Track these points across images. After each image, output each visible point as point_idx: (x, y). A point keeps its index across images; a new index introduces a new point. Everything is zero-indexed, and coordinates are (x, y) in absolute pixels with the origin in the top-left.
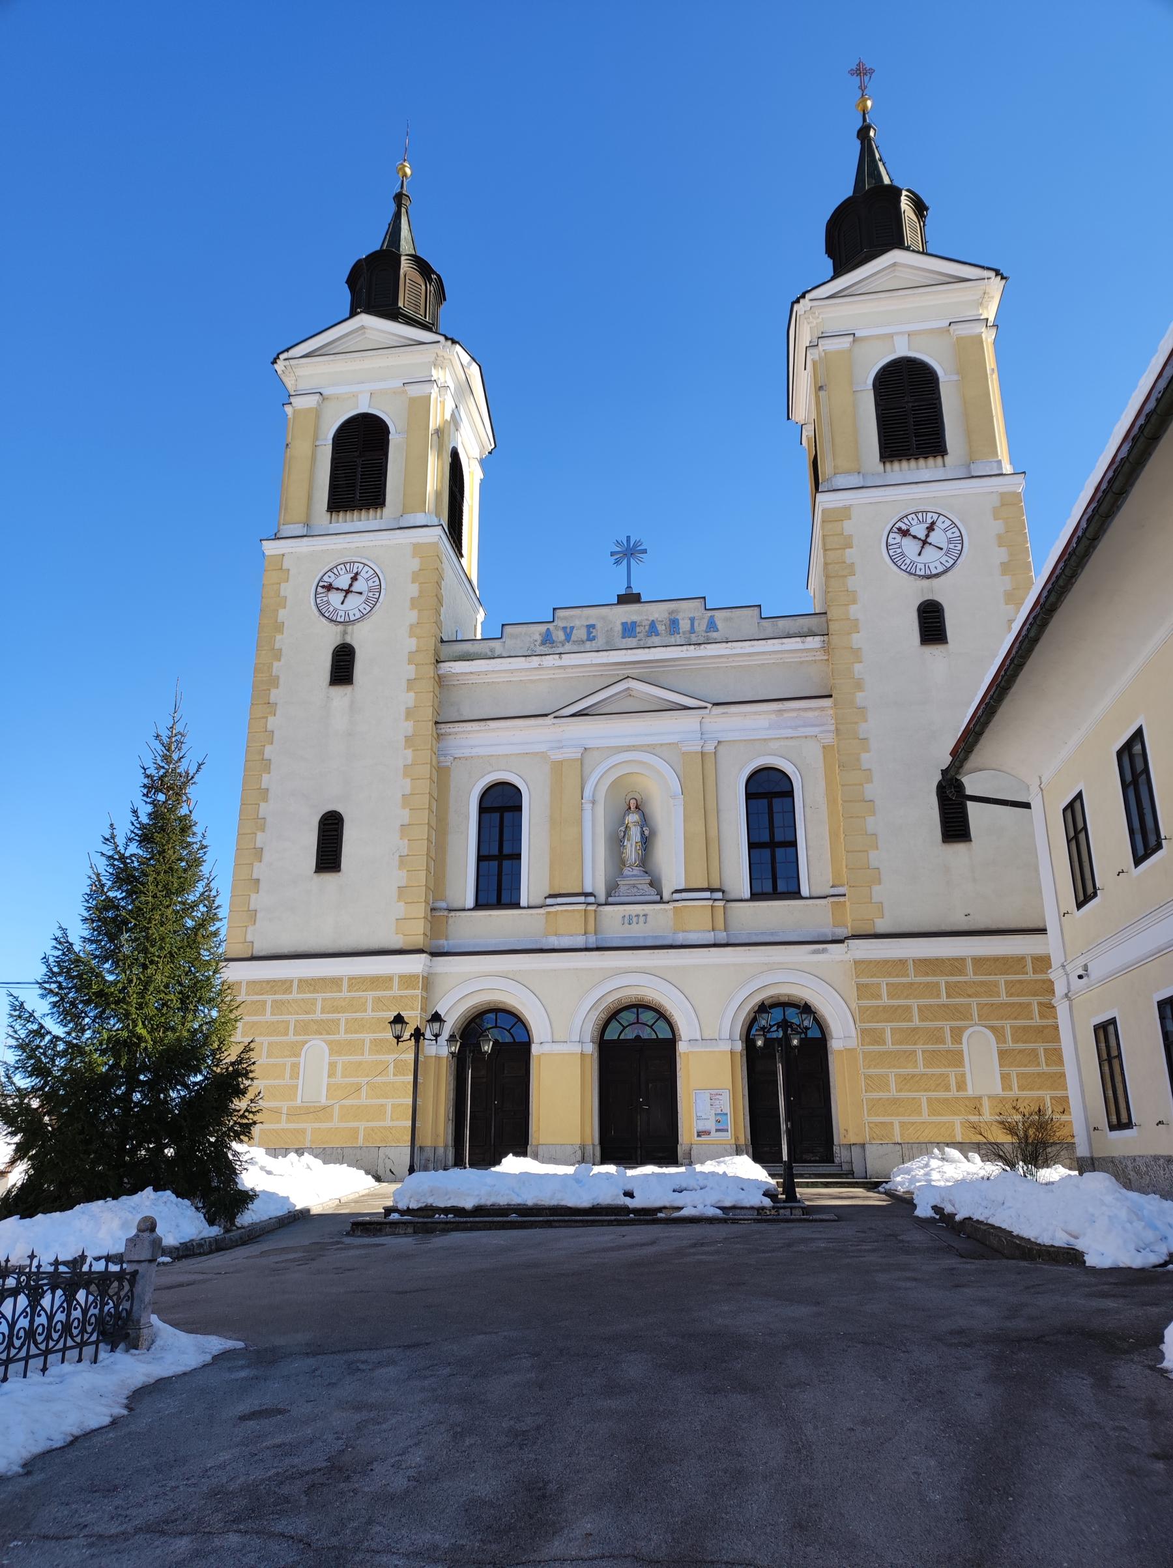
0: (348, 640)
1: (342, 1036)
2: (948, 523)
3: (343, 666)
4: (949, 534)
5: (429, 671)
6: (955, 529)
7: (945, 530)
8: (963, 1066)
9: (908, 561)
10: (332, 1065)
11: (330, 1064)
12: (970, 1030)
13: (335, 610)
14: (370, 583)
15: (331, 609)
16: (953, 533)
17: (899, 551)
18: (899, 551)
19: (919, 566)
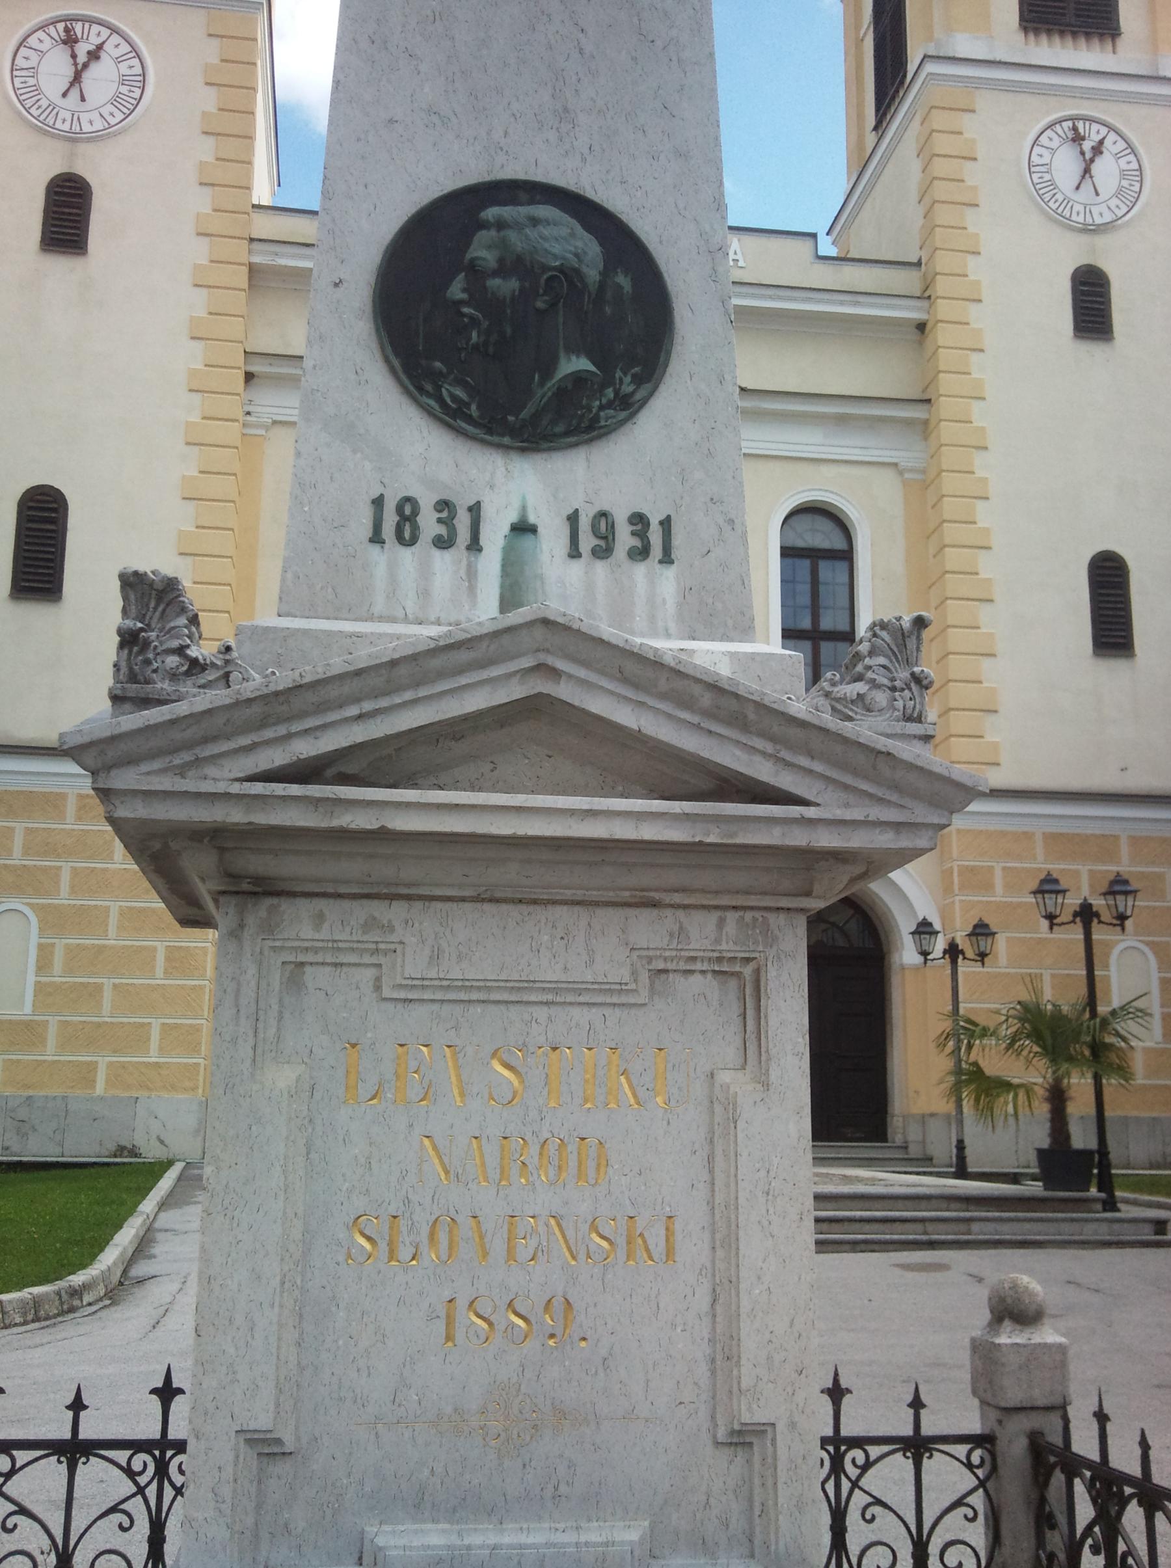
0: (81, 169)
1: (64, 898)
2: (125, 48)
3: (66, 216)
4: (124, 68)
5: (943, 309)
6: (136, 62)
7: (118, 61)
8: (37, 983)
9: (1060, 197)
10: (45, 952)
11: (41, 947)
12: (1122, 946)
13: (52, 106)
14: (124, 68)
15: (44, 103)
16: (131, 67)
17: (1047, 177)
18: (1047, 177)
19: (1077, 207)
